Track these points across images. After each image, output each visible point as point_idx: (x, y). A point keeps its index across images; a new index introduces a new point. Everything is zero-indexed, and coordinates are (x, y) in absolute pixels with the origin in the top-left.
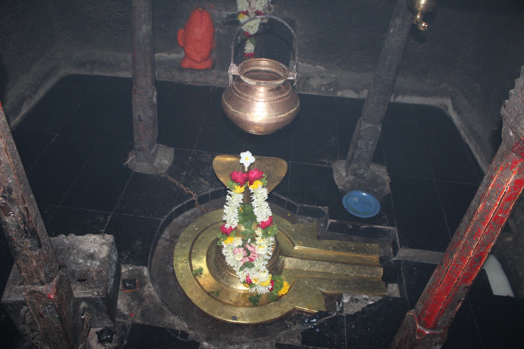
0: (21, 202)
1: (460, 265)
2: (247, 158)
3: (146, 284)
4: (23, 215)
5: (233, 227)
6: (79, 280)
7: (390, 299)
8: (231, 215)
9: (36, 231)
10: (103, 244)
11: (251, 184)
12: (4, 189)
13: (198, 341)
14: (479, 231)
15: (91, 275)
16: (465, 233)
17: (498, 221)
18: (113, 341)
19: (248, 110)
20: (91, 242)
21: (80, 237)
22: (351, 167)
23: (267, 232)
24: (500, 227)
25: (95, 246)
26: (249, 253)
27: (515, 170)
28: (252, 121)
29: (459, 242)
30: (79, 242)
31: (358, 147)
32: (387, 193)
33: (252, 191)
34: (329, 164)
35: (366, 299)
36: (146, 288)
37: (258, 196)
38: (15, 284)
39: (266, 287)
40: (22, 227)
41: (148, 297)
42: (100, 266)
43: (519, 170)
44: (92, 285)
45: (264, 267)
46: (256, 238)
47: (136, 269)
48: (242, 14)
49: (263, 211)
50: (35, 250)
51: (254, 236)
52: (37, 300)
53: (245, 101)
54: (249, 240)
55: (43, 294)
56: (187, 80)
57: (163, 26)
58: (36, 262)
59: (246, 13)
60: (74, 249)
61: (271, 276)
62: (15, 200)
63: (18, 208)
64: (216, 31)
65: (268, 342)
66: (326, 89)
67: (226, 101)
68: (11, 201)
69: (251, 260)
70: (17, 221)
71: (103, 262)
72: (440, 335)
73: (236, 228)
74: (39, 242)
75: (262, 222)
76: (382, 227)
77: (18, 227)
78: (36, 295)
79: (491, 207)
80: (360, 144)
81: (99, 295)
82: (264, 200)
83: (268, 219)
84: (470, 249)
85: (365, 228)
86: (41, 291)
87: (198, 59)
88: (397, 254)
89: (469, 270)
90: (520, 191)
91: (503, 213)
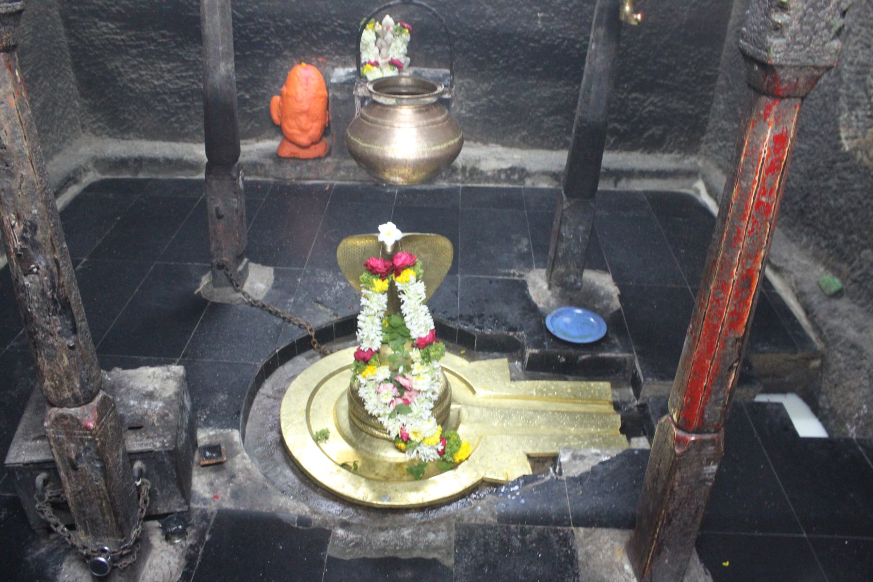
0: (49, 250)
1: (722, 299)
2: (389, 233)
3: (238, 453)
4: (51, 271)
5: (374, 349)
6: (131, 428)
7: (636, 452)
9: (69, 303)
10: (168, 378)
11: (398, 274)
12: (25, 225)
13: (327, 528)
14: (739, 232)
15: (151, 420)
16: (721, 242)
17: (763, 209)
18: (188, 537)
19: (386, 141)
20: (149, 377)
21: (130, 372)
22: (555, 272)
23: (428, 354)
24: (767, 220)
25: (155, 383)
26: (402, 388)
27: (771, 119)
28: (393, 157)
29: (715, 262)
30: (129, 377)
32: (615, 309)
33: (399, 288)
34: (521, 276)
35: (598, 455)
36: (238, 459)
37: (411, 296)
38: (26, 440)
39: (432, 447)
40: (49, 293)
41: (241, 471)
42: (164, 408)
43: (776, 120)
44: (151, 434)
45: (430, 413)
46: (412, 366)
47: (221, 434)
48: (369, 66)
50: (68, 337)
51: (408, 362)
52: (67, 434)
53: (380, 129)
54: (401, 370)
55: (77, 420)
56: (288, 177)
57: (247, 97)
58: (69, 359)
59: (376, 64)
60: (121, 387)
61: (440, 428)
62: (40, 244)
63: (45, 258)
64: (330, 95)
65: (442, 524)
67: (352, 134)
68: (35, 245)
69: (407, 402)
70: (41, 282)
71: (168, 402)
72: (712, 442)
73: (378, 352)
74: (74, 323)
75: (420, 339)
76: (613, 355)
77: (43, 294)
78: (66, 422)
79: (749, 188)
80: (566, 231)
81: (163, 446)
82: (420, 301)
83: (428, 333)
84: (731, 266)
85: (584, 361)
86: (73, 414)
87: (304, 140)
88: (641, 393)
89: (735, 305)
90: (784, 155)
91: (767, 194)
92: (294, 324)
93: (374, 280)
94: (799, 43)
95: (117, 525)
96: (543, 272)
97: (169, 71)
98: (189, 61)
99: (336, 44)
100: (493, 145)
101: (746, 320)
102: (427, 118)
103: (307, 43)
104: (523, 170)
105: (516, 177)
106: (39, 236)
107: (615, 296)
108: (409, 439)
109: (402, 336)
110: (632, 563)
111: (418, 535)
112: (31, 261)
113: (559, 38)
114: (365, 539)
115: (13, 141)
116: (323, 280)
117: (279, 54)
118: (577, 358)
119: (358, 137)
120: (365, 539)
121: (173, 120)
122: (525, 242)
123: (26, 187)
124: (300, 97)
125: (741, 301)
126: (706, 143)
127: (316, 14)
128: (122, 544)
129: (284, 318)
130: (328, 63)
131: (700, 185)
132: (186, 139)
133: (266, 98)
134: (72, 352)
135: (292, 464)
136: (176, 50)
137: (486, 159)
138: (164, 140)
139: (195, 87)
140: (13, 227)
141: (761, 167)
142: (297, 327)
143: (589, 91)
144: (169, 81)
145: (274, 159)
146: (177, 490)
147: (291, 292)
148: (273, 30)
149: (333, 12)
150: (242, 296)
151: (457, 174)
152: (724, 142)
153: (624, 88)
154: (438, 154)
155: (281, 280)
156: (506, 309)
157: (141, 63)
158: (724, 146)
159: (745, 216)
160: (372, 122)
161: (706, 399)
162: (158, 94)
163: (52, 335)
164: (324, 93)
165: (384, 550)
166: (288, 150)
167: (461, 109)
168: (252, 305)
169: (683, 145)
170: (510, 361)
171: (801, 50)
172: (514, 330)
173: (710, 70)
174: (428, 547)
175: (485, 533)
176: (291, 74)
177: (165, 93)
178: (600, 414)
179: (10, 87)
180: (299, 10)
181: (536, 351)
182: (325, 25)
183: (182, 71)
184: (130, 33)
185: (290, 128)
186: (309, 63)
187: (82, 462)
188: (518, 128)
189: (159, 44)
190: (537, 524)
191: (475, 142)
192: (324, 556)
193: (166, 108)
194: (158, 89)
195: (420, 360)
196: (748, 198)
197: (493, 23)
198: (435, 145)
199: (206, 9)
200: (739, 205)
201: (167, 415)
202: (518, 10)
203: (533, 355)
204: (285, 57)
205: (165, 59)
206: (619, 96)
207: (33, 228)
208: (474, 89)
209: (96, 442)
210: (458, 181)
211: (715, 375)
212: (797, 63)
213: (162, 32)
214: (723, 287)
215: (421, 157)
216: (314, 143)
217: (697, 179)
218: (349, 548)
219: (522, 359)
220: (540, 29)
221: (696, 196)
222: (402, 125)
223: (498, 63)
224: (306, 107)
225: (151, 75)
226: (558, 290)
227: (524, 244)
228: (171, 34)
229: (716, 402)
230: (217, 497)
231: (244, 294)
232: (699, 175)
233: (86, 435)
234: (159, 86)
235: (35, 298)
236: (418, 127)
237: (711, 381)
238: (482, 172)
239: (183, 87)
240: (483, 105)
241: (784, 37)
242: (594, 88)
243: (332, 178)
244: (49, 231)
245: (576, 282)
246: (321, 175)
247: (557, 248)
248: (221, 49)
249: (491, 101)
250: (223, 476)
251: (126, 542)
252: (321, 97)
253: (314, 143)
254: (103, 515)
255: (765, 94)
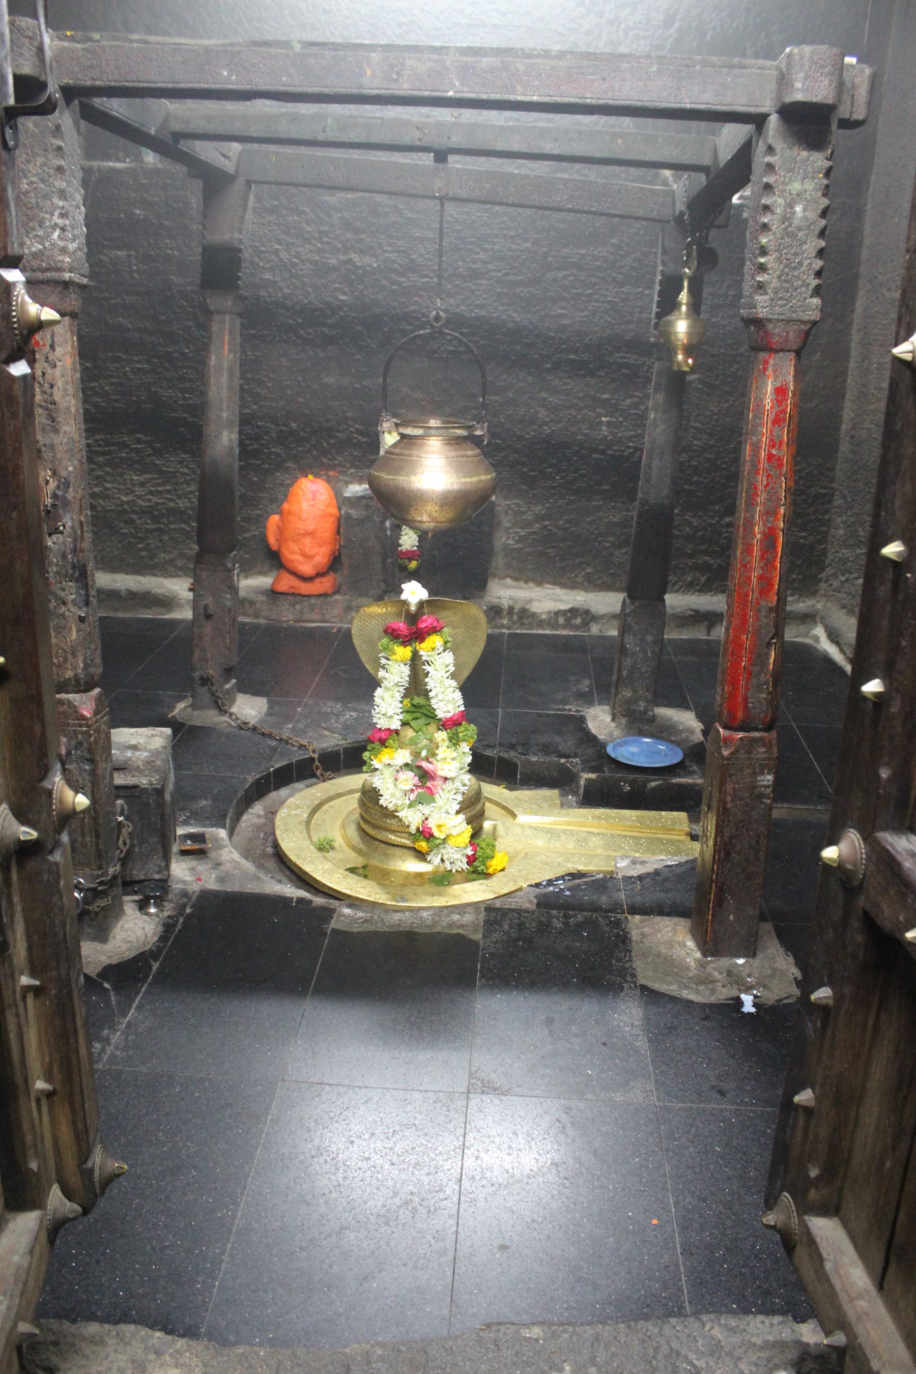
0: (77, 510)
4: (75, 532)
8: (388, 707)
11: (422, 639)
14: (756, 488)
19: (413, 472)
24: (781, 475)
27: (769, 372)
28: (419, 487)
31: (627, 650)
33: (424, 658)
34: (578, 711)
40: (69, 556)
46: (437, 752)
49: (447, 699)
50: (80, 608)
53: (406, 461)
55: (74, 706)
56: (284, 619)
58: (77, 632)
63: (72, 518)
64: (343, 512)
66: (568, 621)
68: (66, 503)
70: (64, 543)
76: (690, 781)
77: (64, 556)
81: (151, 784)
82: (448, 674)
85: (655, 788)
86: (72, 700)
87: (307, 569)
89: (762, 568)
91: (777, 446)
92: (293, 745)
93: (395, 648)
94: (781, 298)
95: (98, 850)
96: (607, 708)
97: (142, 484)
98: (167, 472)
99: (351, 454)
100: (551, 586)
101: (776, 587)
102: (456, 451)
103: (315, 452)
104: (587, 612)
105: (578, 621)
106: (70, 495)
107: (698, 730)
108: (432, 835)
109: (426, 715)
110: (695, 937)
111: (440, 916)
112: (58, 518)
113: (629, 447)
114: (376, 917)
115: (63, 398)
116: (329, 710)
117: (279, 466)
118: (645, 786)
119: (383, 471)
120: (376, 917)
121: (141, 546)
122: (586, 682)
123: (68, 443)
124: (304, 516)
125: (769, 565)
126: (826, 582)
127: (329, 416)
128: (98, 876)
129: (281, 740)
130: (341, 478)
131: (819, 631)
132: (155, 572)
133: (261, 521)
134: (82, 626)
135: (287, 872)
136: (153, 458)
137: (540, 601)
138: (127, 573)
139: (172, 504)
140: (47, 482)
141: (767, 419)
142: (296, 748)
143: (650, 468)
144: (140, 497)
145: (268, 595)
146: (159, 847)
147: (288, 719)
148: (274, 435)
149: (349, 415)
150: (228, 720)
151: (501, 617)
152: (847, 575)
153: (714, 511)
154: (469, 487)
155: (276, 708)
156: (557, 739)
157: (108, 473)
158: (847, 580)
159: (759, 470)
160: (397, 455)
161: (747, 682)
162: (125, 512)
163: (64, 603)
164: (335, 511)
165: (399, 926)
166: (287, 583)
167: (508, 538)
168: (241, 728)
169: (796, 585)
170: (562, 795)
171: (784, 305)
172: (567, 756)
173: (823, 487)
174: (451, 925)
175: (521, 916)
176: (299, 481)
177: (134, 512)
178: (672, 842)
179: (69, 348)
180: (308, 412)
181: (593, 776)
182: (339, 431)
183: (157, 485)
184: (98, 437)
185: (290, 553)
186: (317, 475)
187: (71, 763)
188: (581, 564)
189: (132, 450)
190: (583, 911)
191: (526, 582)
192: (327, 928)
193: (133, 531)
194: (126, 507)
195: (447, 743)
196: (759, 453)
197: (547, 430)
198: (465, 477)
199: (212, 371)
200: (752, 461)
201: (154, 762)
202: (578, 414)
203: (587, 780)
204: (287, 470)
205: (138, 469)
206: (709, 521)
207: (67, 484)
208: (525, 512)
209: (90, 735)
210: (503, 626)
211: (752, 652)
212: (783, 317)
213: (138, 436)
214: (748, 550)
215: (450, 488)
216: (320, 575)
217: (815, 623)
218: (357, 923)
219: (575, 793)
220: (606, 436)
221: (815, 645)
222: (429, 456)
223: (553, 479)
224: (311, 528)
225: (119, 489)
226: (624, 721)
227: (585, 685)
228: (148, 439)
229: (759, 687)
230: (199, 879)
231: (231, 715)
232: (818, 620)
233: (80, 726)
234: (128, 502)
235: (55, 560)
236: (447, 457)
237: (750, 659)
238: (534, 614)
239: (158, 504)
240: (534, 533)
241: (767, 294)
242: (655, 463)
243: (341, 621)
244: (80, 492)
245: (646, 711)
246: (327, 617)
247: (619, 666)
248: (225, 415)
249: (545, 527)
250: (206, 863)
251: (102, 875)
252: (331, 515)
253: (320, 575)
254: (83, 835)
255: (761, 350)
